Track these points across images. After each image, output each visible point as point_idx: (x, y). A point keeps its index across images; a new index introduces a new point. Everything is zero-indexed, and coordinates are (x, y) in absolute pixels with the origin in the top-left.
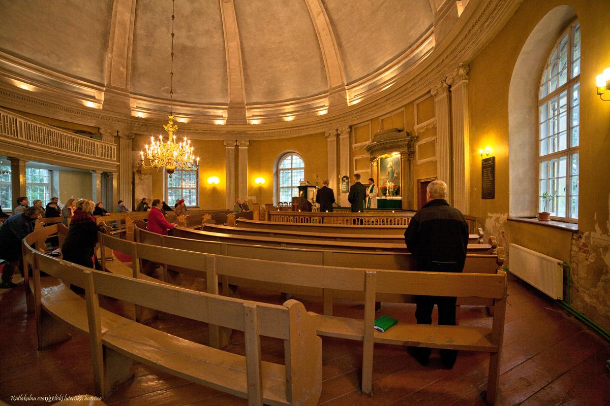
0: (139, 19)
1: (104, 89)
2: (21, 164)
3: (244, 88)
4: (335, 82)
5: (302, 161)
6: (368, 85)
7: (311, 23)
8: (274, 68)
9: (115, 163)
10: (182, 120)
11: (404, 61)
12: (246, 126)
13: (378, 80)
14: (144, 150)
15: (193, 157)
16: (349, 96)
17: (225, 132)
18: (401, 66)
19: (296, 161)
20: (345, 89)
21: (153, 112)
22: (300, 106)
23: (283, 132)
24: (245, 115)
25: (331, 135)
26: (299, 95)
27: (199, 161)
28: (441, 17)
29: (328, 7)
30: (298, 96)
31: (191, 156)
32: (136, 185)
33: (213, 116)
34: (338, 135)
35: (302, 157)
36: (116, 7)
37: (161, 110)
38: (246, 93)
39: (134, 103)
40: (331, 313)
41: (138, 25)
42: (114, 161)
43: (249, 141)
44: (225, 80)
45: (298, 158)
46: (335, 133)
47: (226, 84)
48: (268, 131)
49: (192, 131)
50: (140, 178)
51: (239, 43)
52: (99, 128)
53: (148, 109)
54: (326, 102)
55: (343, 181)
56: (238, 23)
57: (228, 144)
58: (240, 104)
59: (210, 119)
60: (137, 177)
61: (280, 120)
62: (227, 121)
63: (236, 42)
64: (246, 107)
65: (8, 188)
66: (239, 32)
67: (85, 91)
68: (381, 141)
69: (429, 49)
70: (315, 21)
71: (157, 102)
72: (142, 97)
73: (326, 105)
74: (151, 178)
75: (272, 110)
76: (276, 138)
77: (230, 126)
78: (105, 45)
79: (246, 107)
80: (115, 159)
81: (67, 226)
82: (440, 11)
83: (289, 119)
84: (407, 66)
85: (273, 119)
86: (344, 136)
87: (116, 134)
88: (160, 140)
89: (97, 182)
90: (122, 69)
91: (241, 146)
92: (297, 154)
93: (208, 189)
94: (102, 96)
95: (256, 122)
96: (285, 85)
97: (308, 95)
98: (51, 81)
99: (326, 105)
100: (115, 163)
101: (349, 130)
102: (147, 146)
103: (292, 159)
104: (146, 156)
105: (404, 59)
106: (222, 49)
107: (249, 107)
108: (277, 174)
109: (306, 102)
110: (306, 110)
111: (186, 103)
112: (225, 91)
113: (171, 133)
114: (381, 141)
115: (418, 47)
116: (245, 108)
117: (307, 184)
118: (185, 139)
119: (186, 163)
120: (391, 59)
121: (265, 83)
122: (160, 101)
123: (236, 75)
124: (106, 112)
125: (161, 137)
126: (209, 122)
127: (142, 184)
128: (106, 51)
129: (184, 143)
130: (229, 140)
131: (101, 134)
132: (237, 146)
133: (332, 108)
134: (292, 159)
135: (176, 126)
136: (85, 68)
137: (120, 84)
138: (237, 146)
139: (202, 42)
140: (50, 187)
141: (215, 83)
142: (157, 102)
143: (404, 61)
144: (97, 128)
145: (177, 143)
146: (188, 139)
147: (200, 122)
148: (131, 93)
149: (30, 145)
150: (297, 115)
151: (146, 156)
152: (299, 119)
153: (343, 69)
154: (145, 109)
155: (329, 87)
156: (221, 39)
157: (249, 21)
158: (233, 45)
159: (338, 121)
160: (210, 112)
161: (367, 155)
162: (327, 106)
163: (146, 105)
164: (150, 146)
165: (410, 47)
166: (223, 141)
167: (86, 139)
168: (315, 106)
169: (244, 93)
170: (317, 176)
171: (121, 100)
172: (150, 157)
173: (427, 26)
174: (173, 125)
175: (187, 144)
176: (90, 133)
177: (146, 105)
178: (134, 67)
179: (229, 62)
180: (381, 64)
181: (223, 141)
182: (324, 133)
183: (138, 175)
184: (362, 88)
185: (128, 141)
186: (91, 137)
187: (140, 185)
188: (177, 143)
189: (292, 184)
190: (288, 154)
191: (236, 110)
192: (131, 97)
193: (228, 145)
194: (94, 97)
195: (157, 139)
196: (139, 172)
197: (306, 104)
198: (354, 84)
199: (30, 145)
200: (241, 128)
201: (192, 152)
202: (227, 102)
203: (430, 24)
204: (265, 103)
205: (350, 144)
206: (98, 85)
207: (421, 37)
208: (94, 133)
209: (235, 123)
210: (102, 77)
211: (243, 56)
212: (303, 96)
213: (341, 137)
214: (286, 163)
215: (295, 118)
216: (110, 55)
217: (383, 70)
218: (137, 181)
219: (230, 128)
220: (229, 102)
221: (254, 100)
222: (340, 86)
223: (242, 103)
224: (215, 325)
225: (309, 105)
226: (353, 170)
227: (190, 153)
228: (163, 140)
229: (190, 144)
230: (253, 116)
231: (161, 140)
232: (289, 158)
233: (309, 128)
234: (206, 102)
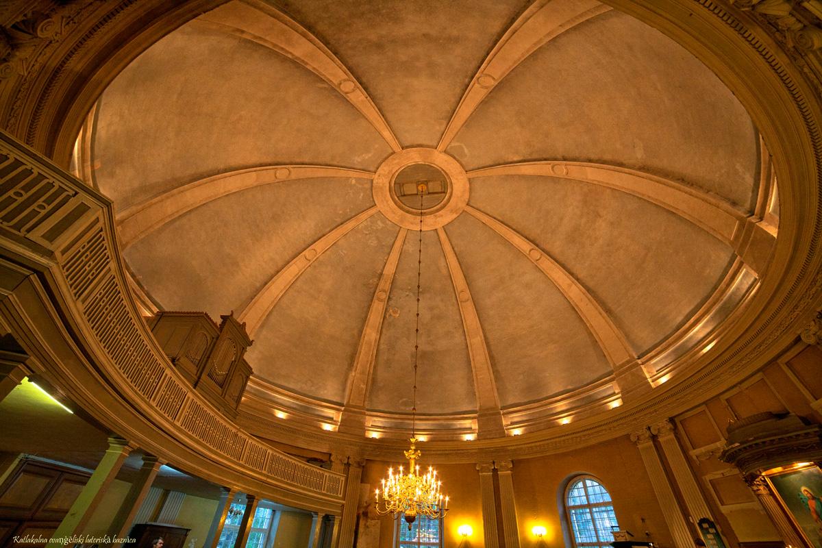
0: (383, 335)
1: (343, 408)
2: (255, 503)
3: (495, 387)
4: (619, 356)
5: (604, 491)
6: (673, 352)
7: (563, 298)
8: (530, 356)
9: (340, 501)
10: (422, 438)
11: (717, 307)
12: (503, 439)
13: (687, 341)
14: (381, 489)
15: (441, 497)
16: (649, 372)
17: (476, 451)
18: (715, 314)
19: (594, 491)
20: (637, 365)
21: (389, 431)
22: (578, 400)
23: (560, 442)
24: (501, 425)
25: (642, 437)
27: (448, 501)
29: (579, 277)
30: (570, 387)
31: (438, 495)
32: (359, 536)
33: (460, 429)
34: (654, 438)
35: (602, 482)
36: (366, 331)
37: (397, 427)
38: (499, 394)
39: (370, 421)
41: (382, 341)
42: (339, 498)
43: (512, 461)
44: (470, 380)
45: (595, 484)
46: (648, 434)
47: (472, 385)
48: (538, 444)
49: (433, 452)
50: (365, 525)
51: (483, 338)
52: (330, 455)
53: (384, 428)
55: (706, 532)
56: (479, 318)
57: (482, 468)
58: (492, 409)
59: (456, 434)
60: (362, 523)
61: (552, 425)
62: (478, 435)
63: (479, 338)
64: (502, 412)
65: (231, 534)
66: (482, 326)
67: (327, 412)
68: (748, 441)
69: (750, 283)
70: (567, 294)
71: (394, 418)
72: (379, 414)
73: (616, 392)
74: (379, 525)
75: (537, 412)
76: (552, 453)
77: (483, 442)
78: (351, 365)
79: (502, 412)
80: (341, 496)
82: (737, 237)
83: (565, 421)
84: (725, 312)
85: (542, 424)
86: (666, 438)
87: (346, 462)
88: (399, 472)
89: (317, 528)
90: (363, 386)
91: (502, 471)
92: (593, 478)
93: (459, 544)
94: (338, 417)
95: (517, 432)
96: (548, 375)
97: (585, 383)
98: (302, 406)
99: (616, 392)
100: (340, 501)
101: (670, 426)
102: (383, 481)
103: (585, 487)
104: (381, 496)
105: (715, 303)
106: (464, 347)
107: (505, 411)
108: (566, 517)
109: (585, 392)
110: (587, 405)
111: (426, 416)
112: (472, 394)
113: (413, 462)
114: (748, 441)
115: (728, 285)
116: (499, 413)
117: (628, 538)
118: (430, 469)
119: (430, 506)
120: (692, 311)
121: (521, 377)
122: (397, 416)
123: (484, 374)
124: (342, 434)
125: (401, 468)
126: (455, 438)
127: (366, 534)
128: (351, 370)
129: (429, 475)
131: (331, 461)
132: (495, 470)
133: (626, 396)
134: (585, 487)
135: (419, 451)
136: (330, 390)
137: (359, 402)
138: (495, 470)
139: (442, 344)
140: (267, 534)
141: (458, 387)
142: (394, 418)
143: (717, 307)
144: (327, 453)
145: (420, 476)
146: (434, 469)
147: (443, 439)
148: (368, 410)
149: (268, 480)
150: (575, 413)
151: (381, 496)
152: (580, 420)
154: (380, 427)
155: (612, 365)
156: (463, 337)
157: (491, 313)
158: (477, 341)
159: (646, 412)
160: (455, 425)
161: (731, 471)
162: (618, 394)
163: (382, 422)
164: (387, 481)
165: (715, 288)
166: (475, 464)
167: (315, 469)
169: (496, 394)
170: (643, 520)
171: (357, 419)
172: (386, 496)
173: (727, 259)
174: (416, 450)
175: (433, 475)
176: (322, 461)
177: (382, 422)
178: (374, 381)
179: (474, 360)
180: (680, 319)
181: (475, 464)
182: (628, 436)
183: (363, 520)
184: (665, 357)
185: (358, 469)
186: (321, 466)
187: (363, 536)
188: (420, 476)
189: (597, 537)
190: (575, 479)
191: (489, 418)
192: (367, 415)
193: (482, 470)
194: (331, 419)
195: (396, 472)
196: (366, 514)
197: (584, 395)
198: (649, 355)
199: (268, 480)
200: (498, 443)
201: (439, 489)
202: (475, 409)
203: (730, 255)
204: (529, 403)
206: (337, 405)
208: (322, 461)
209: (488, 437)
210: (343, 397)
211: (490, 352)
212: (578, 385)
213: (661, 440)
214: (577, 495)
215: (574, 418)
216: (353, 374)
217: (687, 325)
218: (361, 530)
219: (484, 444)
220: (478, 409)
221: (511, 401)
222: (628, 362)
223: (495, 408)
225: (590, 396)
226: (718, 508)
227: (437, 489)
228: (403, 472)
229: (436, 476)
230: (512, 423)
231: (401, 472)
232: (580, 485)
234: (450, 412)
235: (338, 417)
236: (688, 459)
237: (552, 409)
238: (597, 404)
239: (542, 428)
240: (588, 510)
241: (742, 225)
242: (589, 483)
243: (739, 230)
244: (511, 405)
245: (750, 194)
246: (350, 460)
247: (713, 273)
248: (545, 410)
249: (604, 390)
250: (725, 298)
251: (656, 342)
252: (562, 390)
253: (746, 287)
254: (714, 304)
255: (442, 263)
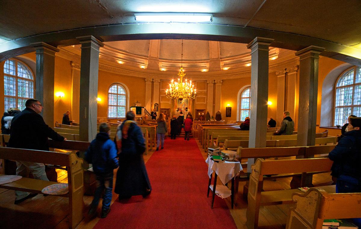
13: (177, 65)
17: (73, 54)
23: (117, 69)
26: (129, 50)
28: (214, 61)
30: (127, 51)
35: (111, 86)
37: (172, 66)
40: (248, 131)
54: (146, 62)
57: (76, 65)
76: (111, 72)
81: (167, 118)
83: (120, 62)
94: (208, 65)
103: (117, 88)
130: (77, 63)
134: (117, 88)
150: (126, 62)
153: (159, 50)
168: (138, 61)
205: (160, 89)
207: (201, 60)
212: (131, 52)
213: (154, 83)
214: (113, 89)
215: (125, 63)
219: (148, 71)
222: (156, 58)
224: (249, 133)
225: (134, 59)
233: (136, 73)
235: (208, 65)
236: (160, 90)
237: (116, 54)
238: (135, 63)
239: (109, 60)
240: (116, 95)
241: (217, 59)
242: (119, 87)
243: (216, 58)
244: (143, 55)
245: (225, 56)
246: (215, 81)
247: (198, 57)
248: (113, 53)
249: (140, 60)
250: (195, 64)
251: (168, 59)
252: (124, 50)
253: (202, 66)
254: (192, 63)
255: (355, 195)
